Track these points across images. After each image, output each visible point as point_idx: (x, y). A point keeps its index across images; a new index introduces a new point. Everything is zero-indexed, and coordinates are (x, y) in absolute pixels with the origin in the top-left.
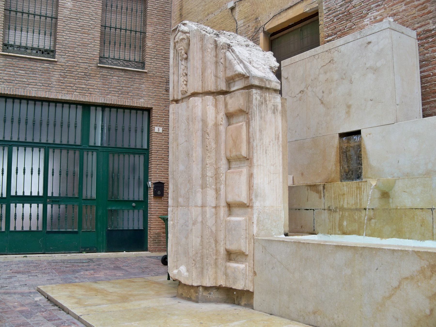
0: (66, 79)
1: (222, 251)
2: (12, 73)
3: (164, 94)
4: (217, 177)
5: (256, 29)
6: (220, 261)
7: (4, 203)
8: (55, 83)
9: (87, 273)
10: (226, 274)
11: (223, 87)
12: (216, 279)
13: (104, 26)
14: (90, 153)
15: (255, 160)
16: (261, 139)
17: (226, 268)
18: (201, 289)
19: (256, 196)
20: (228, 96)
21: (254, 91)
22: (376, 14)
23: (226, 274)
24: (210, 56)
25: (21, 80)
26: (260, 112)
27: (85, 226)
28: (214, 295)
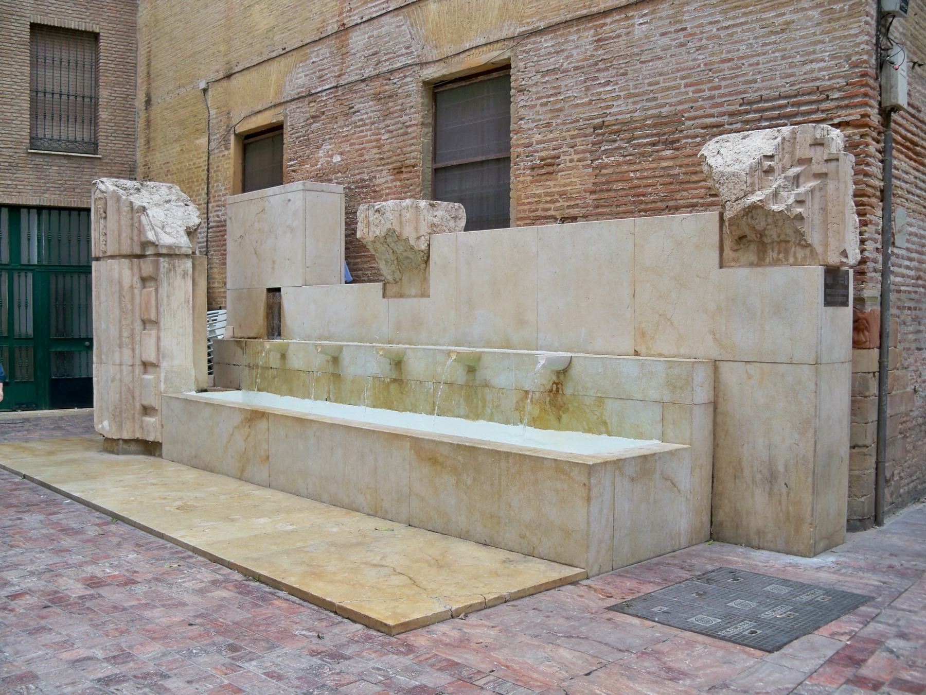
1: (138, 406)
4: (132, 336)
5: (228, 126)
6: (137, 415)
9: (19, 434)
10: (142, 427)
11: (138, 251)
12: (134, 432)
13: (34, 91)
14: (23, 274)
15: (162, 324)
16: (169, 304)
17: (142, 421)
18: (121, 442)
19: (164, 357)
20: (142, 261)
21: (162, 259)
22: (329, 147)
23: (142, 427)
24: (125, 221)
26: (168, 278)
27: (18, 374)
28: (133, 447)
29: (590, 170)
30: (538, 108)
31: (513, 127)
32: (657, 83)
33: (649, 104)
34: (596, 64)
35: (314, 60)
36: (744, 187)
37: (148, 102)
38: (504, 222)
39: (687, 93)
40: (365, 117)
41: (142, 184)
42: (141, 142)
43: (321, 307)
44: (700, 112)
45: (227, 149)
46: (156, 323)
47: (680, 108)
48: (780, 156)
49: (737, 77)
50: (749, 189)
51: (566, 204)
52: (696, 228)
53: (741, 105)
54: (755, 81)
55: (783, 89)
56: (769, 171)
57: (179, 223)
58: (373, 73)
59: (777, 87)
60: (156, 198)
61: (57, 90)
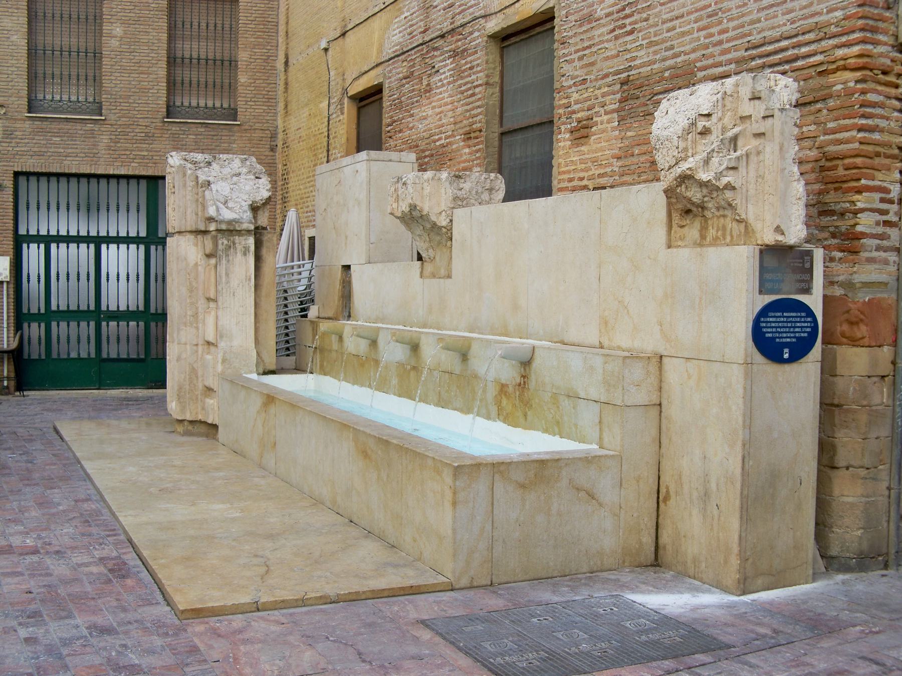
0: (119, 145)
1: (200, 386)
2: (42, 142)
3: (267, 156)
7: (42, 321)
8: (103, 152)
16: (228, 282)
19: (221, 337)
25: (56, 150)
26: (227, 255)
29: (617, 133)
30: (576, 63)
31: (557, 85)
32: (674, 28)
33: (667, 53)
34: (624, 9)
35: (406, 14)
36: (676, 153)
37: (286, 63)
38: (547, 192)
39: (698, 39)
40: (443, 77)
41: (215, 157)
42: (281, 105)
43: (385, 290)
44: (710, 61)
45: (342, 113)
46: (215, 301)
47: (693, 56)
48: (720, 114)
49: (743, 16)
50: (683, 155)
51: (597, 172)
52: (648, 201)
53: (746, 50)
54: (759, 21)
55: (784, 28)
56: (705, 132)
57: (245, 197)
58: (450, 27)
59: (779, 26)
60: (226, 171)
61: (203, 56)
